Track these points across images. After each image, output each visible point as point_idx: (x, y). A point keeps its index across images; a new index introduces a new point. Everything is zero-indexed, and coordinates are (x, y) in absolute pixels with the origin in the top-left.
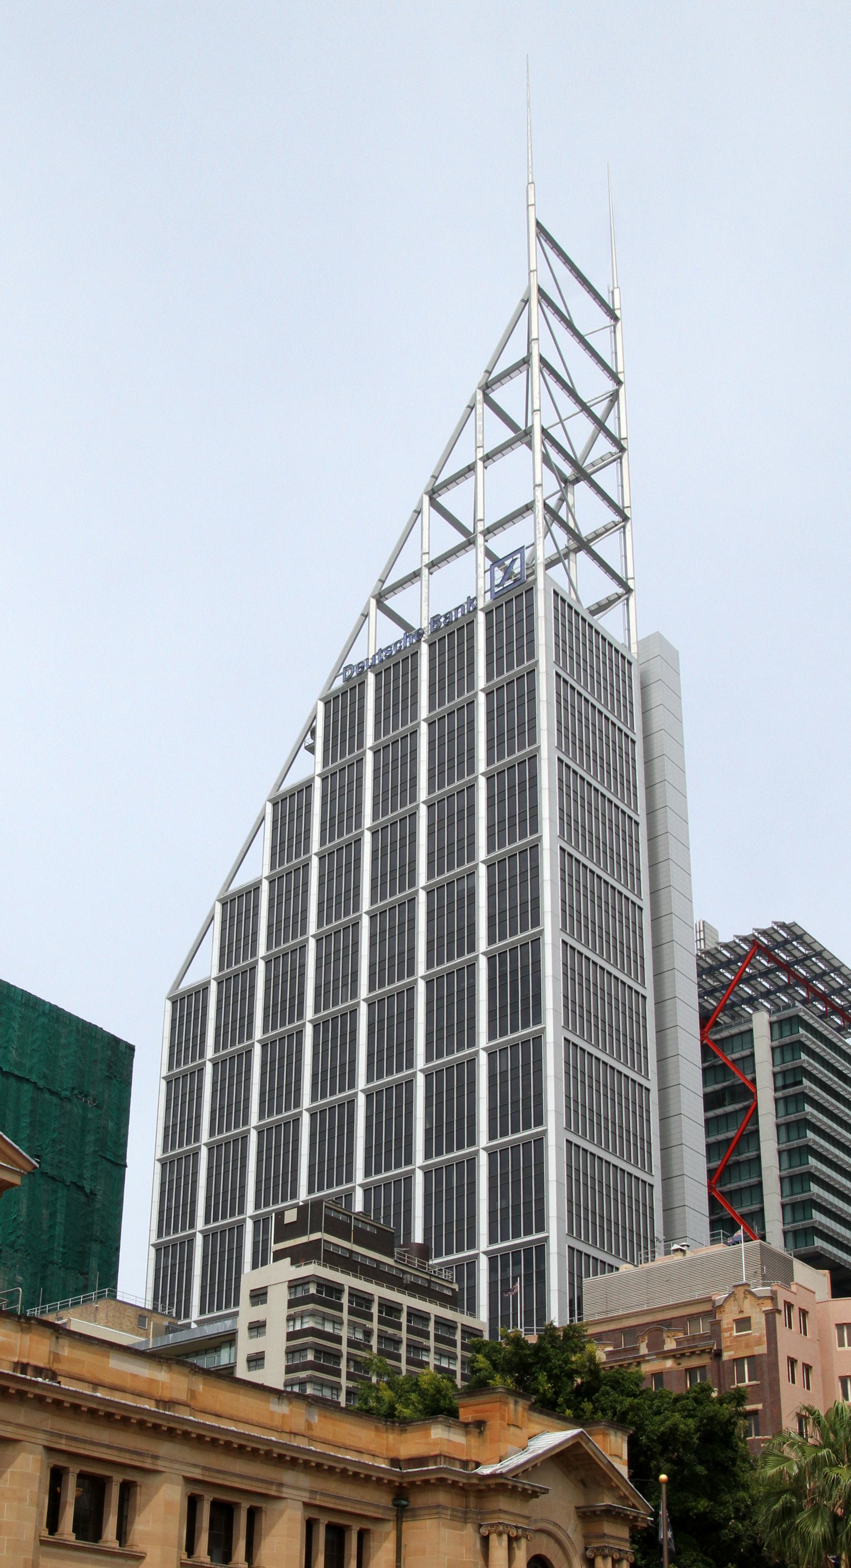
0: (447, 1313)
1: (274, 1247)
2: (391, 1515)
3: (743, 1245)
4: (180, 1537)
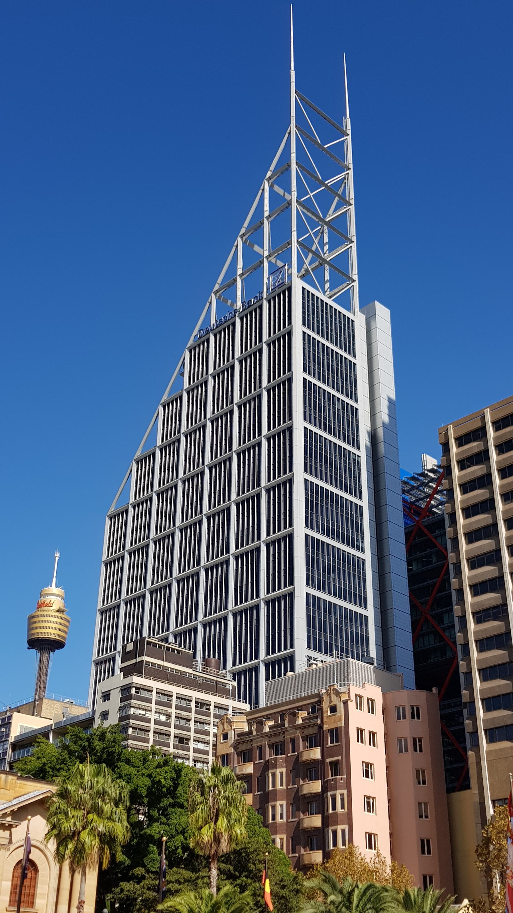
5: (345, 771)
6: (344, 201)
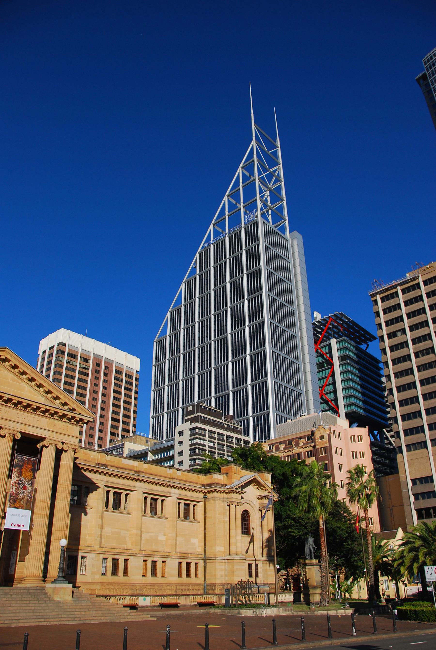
0: (239, 436)
1: (185, 418)
2: (203, 500)
3: (320, 413)
4: (142, 508)
5: (330, 468)
6: (278, 180)
